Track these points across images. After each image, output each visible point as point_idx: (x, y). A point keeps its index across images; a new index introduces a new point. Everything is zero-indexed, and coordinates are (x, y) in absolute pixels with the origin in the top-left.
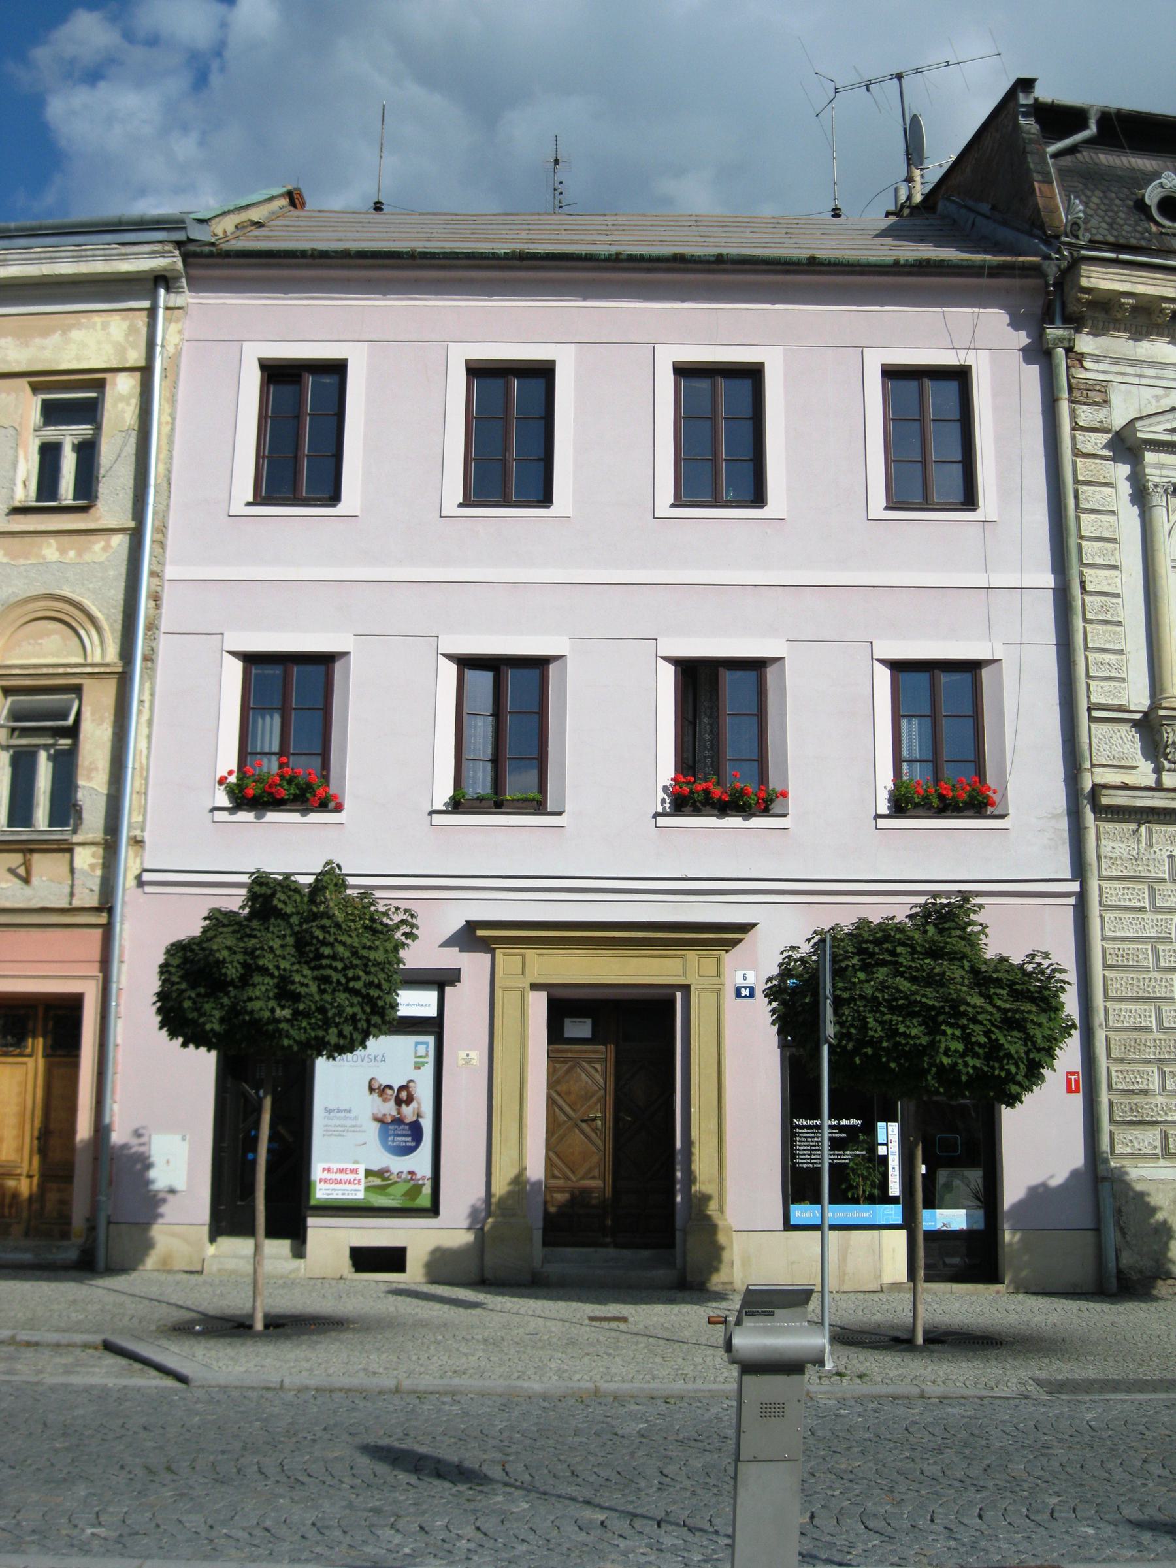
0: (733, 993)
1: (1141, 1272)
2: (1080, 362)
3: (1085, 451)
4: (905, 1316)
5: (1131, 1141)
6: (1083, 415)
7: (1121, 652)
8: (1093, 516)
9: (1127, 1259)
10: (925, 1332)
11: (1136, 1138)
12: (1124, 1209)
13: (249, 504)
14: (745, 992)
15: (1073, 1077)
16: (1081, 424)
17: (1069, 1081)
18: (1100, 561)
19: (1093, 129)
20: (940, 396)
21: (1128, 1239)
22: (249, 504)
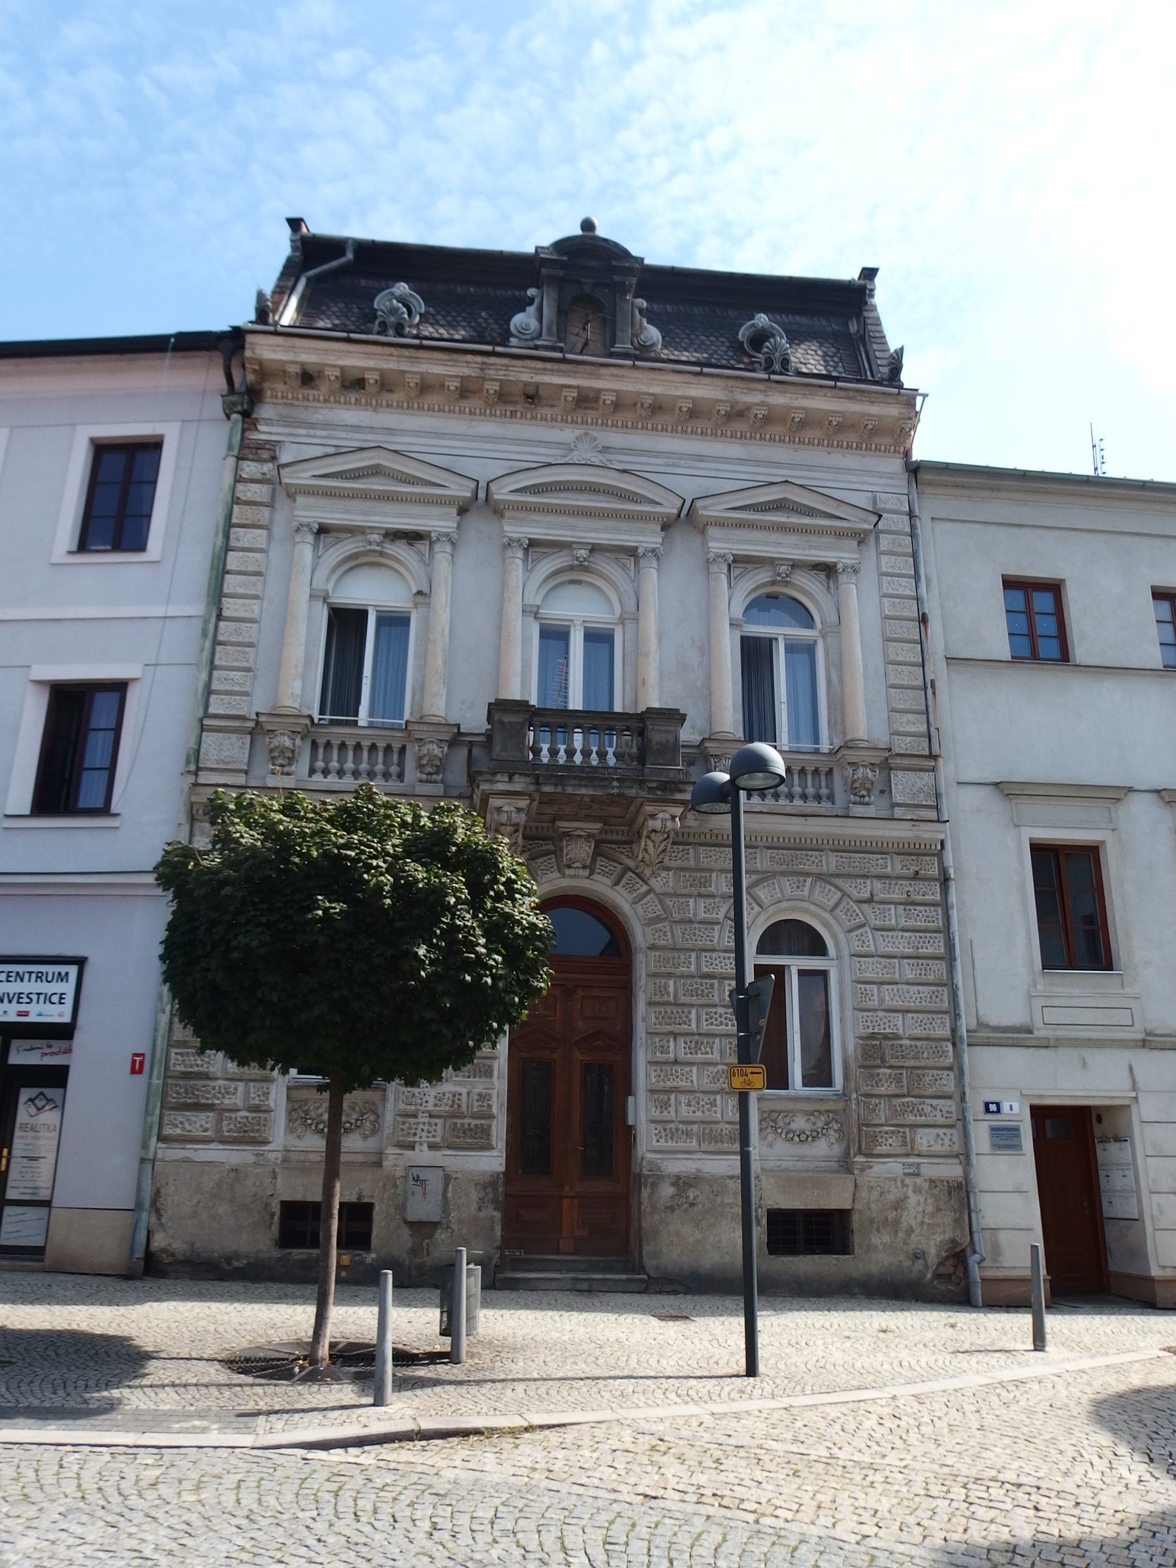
0: (982, 1108)
1: (172, 1254)
2: (255, 425)
3: (243, 498)
4: (371, 1336)
5: (182, 1123)
6: (247, 469)
7: (249, 670)
8: (241, 554)
9: (159, 1241)
10: (332, 1346)
11: (188, 1120)
12: (163, 1191)
13: (70, 553)
14: (993, 1108)
15: (138, 1059)
16: (244, 476)
17: (134, 1062)
18: (241, 591)
19: (350, 256)
20: (1042, 601)
21: (163, 1220)
22: (70, 553)
